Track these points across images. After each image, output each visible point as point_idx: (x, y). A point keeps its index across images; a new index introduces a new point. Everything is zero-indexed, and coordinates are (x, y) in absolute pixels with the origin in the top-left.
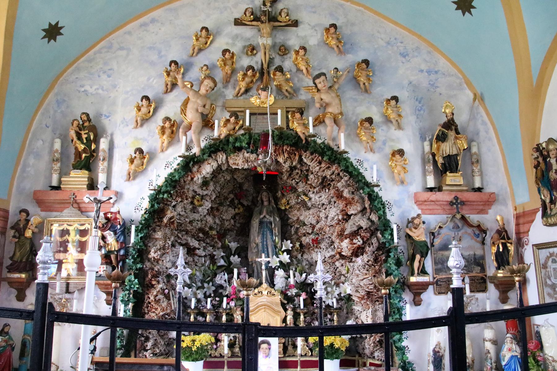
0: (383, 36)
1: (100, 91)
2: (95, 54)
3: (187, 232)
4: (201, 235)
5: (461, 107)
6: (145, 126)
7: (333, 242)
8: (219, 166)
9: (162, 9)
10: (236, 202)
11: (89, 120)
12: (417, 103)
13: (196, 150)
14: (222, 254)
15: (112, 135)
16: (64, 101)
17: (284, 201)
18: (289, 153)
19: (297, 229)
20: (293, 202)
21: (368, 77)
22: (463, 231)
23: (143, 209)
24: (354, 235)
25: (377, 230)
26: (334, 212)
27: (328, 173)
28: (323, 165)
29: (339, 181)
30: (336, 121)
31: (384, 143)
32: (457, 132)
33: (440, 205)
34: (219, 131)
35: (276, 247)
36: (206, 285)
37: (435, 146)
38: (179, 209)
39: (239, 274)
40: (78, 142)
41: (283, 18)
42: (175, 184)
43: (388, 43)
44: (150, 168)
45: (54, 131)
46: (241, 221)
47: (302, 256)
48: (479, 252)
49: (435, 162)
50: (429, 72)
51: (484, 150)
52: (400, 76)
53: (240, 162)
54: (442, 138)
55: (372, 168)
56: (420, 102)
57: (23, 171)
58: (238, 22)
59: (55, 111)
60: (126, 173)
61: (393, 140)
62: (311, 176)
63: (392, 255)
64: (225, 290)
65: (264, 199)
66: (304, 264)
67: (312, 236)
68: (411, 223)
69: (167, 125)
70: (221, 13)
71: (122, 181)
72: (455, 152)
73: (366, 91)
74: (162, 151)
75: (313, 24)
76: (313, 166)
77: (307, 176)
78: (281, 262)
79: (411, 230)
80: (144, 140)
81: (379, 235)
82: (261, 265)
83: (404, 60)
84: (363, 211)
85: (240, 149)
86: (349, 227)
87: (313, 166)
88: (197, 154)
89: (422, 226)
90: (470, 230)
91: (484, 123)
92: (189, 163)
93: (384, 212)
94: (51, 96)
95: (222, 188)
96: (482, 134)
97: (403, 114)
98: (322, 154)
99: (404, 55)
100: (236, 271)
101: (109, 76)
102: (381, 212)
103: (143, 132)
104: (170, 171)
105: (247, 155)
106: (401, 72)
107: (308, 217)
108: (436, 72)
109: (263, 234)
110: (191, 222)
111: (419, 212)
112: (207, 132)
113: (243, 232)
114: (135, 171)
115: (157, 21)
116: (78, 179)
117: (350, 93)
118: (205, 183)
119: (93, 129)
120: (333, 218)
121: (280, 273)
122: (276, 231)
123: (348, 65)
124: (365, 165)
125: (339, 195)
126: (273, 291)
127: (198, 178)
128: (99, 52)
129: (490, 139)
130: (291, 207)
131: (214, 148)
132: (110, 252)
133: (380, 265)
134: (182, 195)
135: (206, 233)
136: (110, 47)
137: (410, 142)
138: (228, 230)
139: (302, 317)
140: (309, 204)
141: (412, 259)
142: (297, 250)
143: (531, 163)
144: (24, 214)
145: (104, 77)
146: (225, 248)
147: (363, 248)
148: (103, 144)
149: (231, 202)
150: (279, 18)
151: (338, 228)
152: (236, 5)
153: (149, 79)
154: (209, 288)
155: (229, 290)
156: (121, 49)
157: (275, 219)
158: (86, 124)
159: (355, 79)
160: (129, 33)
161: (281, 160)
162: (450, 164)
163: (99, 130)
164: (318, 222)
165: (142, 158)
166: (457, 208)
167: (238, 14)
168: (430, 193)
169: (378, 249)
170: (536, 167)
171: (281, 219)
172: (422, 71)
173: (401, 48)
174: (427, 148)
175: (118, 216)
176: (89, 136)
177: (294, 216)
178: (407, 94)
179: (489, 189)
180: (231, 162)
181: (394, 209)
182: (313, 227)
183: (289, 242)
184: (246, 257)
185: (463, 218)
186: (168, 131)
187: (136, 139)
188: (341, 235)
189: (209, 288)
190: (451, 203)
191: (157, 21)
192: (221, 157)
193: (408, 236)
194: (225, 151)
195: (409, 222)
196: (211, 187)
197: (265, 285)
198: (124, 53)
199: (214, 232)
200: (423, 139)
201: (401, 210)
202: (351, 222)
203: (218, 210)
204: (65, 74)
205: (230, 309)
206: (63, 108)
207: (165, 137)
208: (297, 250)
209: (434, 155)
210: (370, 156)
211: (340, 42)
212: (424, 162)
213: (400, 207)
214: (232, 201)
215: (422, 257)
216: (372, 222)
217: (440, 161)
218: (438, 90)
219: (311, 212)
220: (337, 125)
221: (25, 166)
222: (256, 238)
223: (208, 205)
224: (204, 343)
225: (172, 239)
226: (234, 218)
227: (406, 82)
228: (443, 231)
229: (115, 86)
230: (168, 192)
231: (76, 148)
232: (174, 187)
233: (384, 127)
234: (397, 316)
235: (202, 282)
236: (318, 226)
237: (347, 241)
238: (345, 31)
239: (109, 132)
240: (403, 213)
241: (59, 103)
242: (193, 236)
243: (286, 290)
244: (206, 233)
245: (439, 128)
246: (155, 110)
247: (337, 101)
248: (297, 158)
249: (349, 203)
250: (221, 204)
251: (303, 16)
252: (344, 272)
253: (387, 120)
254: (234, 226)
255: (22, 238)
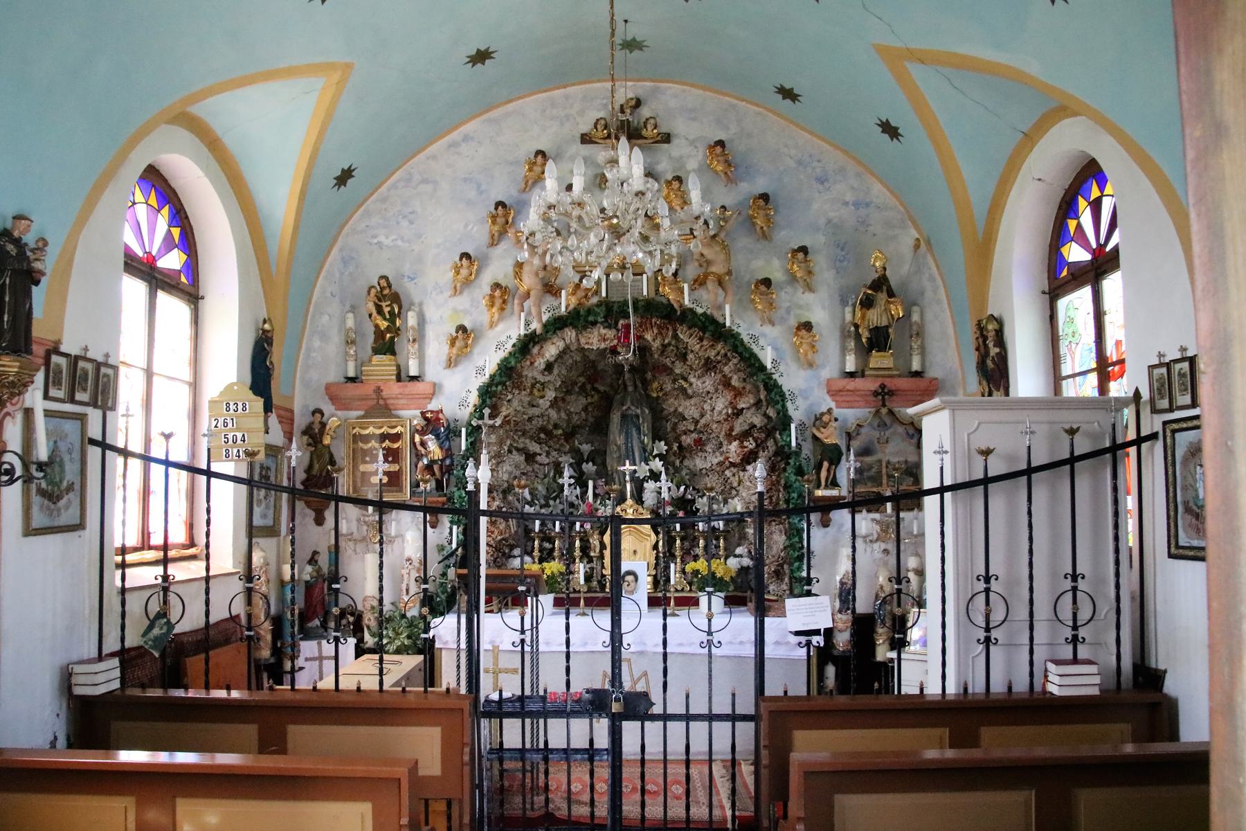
0: (793, 152)
1: (399, 243)
2: (389, 190)
3: (524, 433)
4: (542, 436)
5: (896, 255)
6: (466, 293)
7: (721, 443)
8: (567, 348)
9: (478, 119)
10: (589, 387)
11: (390, 286)
12: (838, 251)
13: (536, 326)
14: (572, 461)
15: (421, 304)
16: (353, 258)
17: (655, 385)
18: (659, 327)
19: (676, 424)
20: (668, 387)
21: (768, 219)
22: (891, 430)
23: (471, 405)
24: (745, 435)
25: (774, 429)
26: (721, 404)
27: (712, 354)
28: (705, 343)
29: (726, 364)
30: (720, 283)
31: (788, 311)
32: (891, 294)
33: (861, 396)
34: (565, 303)
35: (645, 450)
36: (551, 502)
37: (858, 314)
38: (515, 403)
39: (595, 487)
40: (379, 317)
41: (649, 132)
42: (508, 374)
43: (800, 162)
44: (476, 351)
45: (342, 302)
46: (596, 413)
47: (681, 462)
48: (912, 459)
49: (858, 336)
50: (857, 204)
51: (929, 316)
52: (815, 213)
53: (595, 341)
54: (867, 303)
55: (770, 345)
56: (842, 250)
57: (308, 356)
58: (586, 139)
59: (342, 274)
60: (444, 358)
61: (800, 307)
62: (691, 356)
63: (792, 461)
64: (578, 510)
65: (628, 383)
66: (684, 473)
67: (695, 436)
68: (819, 420)
69: (498, 293)
70: (562, 124)
71: (440, 368)
72: (885, 323)
73: (765, 236)
74: (491, 327)
75: (691, 137)
76: (693, 343)
77: (686, 354)
78: (651, 471)
79: (818, 429)
80: (466, 312)
81: (778, 436)
82: (625, 474)
83: (821, 187)
84: (758, 404)
85: (594, 323)
86: (739, 426)
87: (693, 343)
88: (538, 332)
89: (834, 424)
90: (900, 429)
91: (932, 279)
92: (527, 345)
93: (784, 406)
94: (335, 252)
95: (570, 369)
96: (929, 294)
97: (816, 269)
98: (703, 329)
99: (821, 181)
100: (591, 483)
101: (411, 223)
102: (779, 407)
103: (462, 301)
104: (502, 354)
105: (603, 331)
106: (815, 206)
107: (689, 409)
108: (868, 205)
109: (627, 433)
110: (530, 419)
111: (833, 405)
112: (550, 301)
113: (600, 429)
114: (458, 356)
115: (472, 138)
116: (382, 366)
117: (743, 242)
118: (549, 367)
119: (396, 298)
120: (720, 412)
121: (650, 486)
122: (645, 428)
123: (741, 198)
124: (762, 342)
125: (727, 383)
126: (641, 510)
127: (540, 363)
128: (394, 186)
129: (939, 302)
130: (665, 394)
131: (557, 325)
132: (433, 462)
133: (779, 476)
134: (519, 386)
135: (549, 434)
136: (409, 179)
137: (824, 308)
138: (578, 426)
139: (678, 542)
140: (690, 391)
141: (818, 467)
142: (674, 454)
143: (973, 346)
144: (318, 415)
145: (405, 223)
146: (576, 453)
147: (757, 453)
148: (412, 319)
149: (580, 388)
150: (644, 132)
151: (726, 426)
152: (582, 113)
153: (466, 226)
154: (555, 506)
155: (583, 508)
156: (425, 181)
157: (643, 412)
158: (386, 292)
159: (751, 220)
160: (434, 157)
161: (648, 337)
162: (878, 340)
163: (404, 304)
164: (702, 416)
165: (464, 336)
166: (883, 399)
167: (586, 127)
168: (847, 380)
169: (776, 454)
170: (977, 349)
171: (652, 409)
172: (846, 204)
173: (818, 170)
174: (849, 317)
175: (441, 416)
176: (393, 309)
177: (671, 405)
178: (822, 239)
179: (932, 373)
180: (583, 341)
181: (800, 402)
182: (697, 422)
183: (663, 443)
184: (604, 464)
185: (891, 412)
186: (498, 302)
187: (455, 311)
188: (730, 437)
189: (555, 506)
190: (876, 394)
191: (472, 138)
192: (570, 334)
193: (815, 438)
194: (575, 327)
195: (817, 419)
196: (556, 371)
197: (629, 502)
198: (428, 188)
199: (560, 432)
200: (844, 303)
201: (808, 402)
202: (741, 419)
203: (563, 400)
204: (351, 222)
205: (585, 532)
206: (351, 268)
207: (494, 310)
208: (674, 454)
209: (857, 326)
210: (767, 329)
211: (730, 165)
212: (844, 335)
213: (806, 398)
214: (583, 388)
215: (831, 464)
216: (769, 418)
217: (865, 334)
218: (871, 228)
219: (693, 401)
220: (723, 289)
221: (309, 350)
222: (617, 438)
223: (551, 395)
224: (555, 571)
225: (508, 443)
226: (585, 409)
227: (822, 221)
228: (863, 431)
229: (419, 236)
230: (504, 384)
231: (377, 326)
232: (510, 377)
233: (789, 289)
234: (797, 539)
235: (547, 498)
236: (703, 421)
237: (735, 443)
238: (738, 147)
239: (416, 301)
240: (811, 406)
241: (345, 262)
242: (532, 438)
243: (658, 508)
244: (549, 434)
245: (863, 290)
246: (478, 272)
247: (722, 257)
248: (670, 334)
249: (738, 393)
250: (568, 392)
251: (679, 126)
252: (735, 484)
253: (793, 279)
254: (586, 420)
255: (320, 446)
